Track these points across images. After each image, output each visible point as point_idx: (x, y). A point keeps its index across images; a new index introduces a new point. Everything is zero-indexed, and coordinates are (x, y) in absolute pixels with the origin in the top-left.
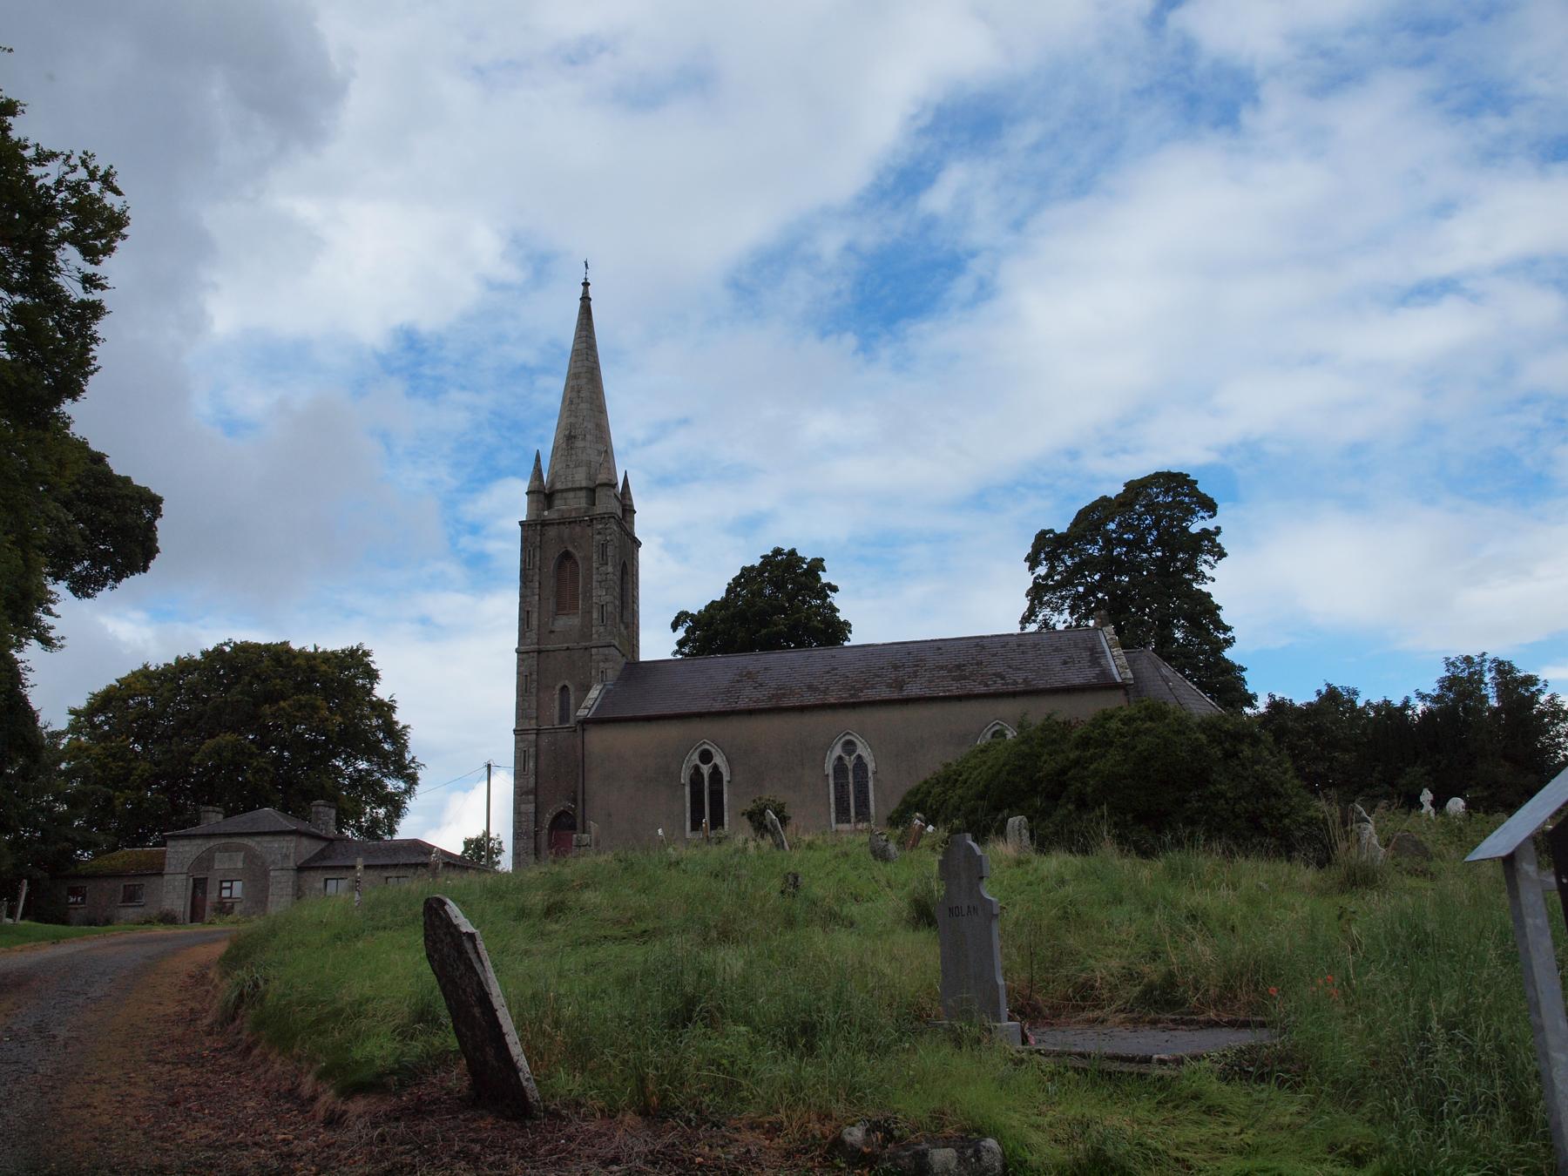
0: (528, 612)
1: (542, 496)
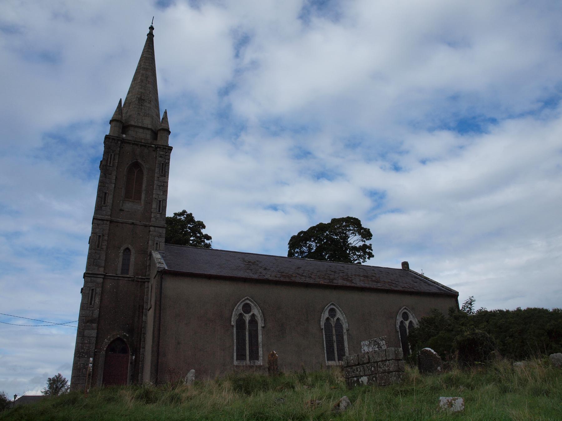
0: (106, 193)
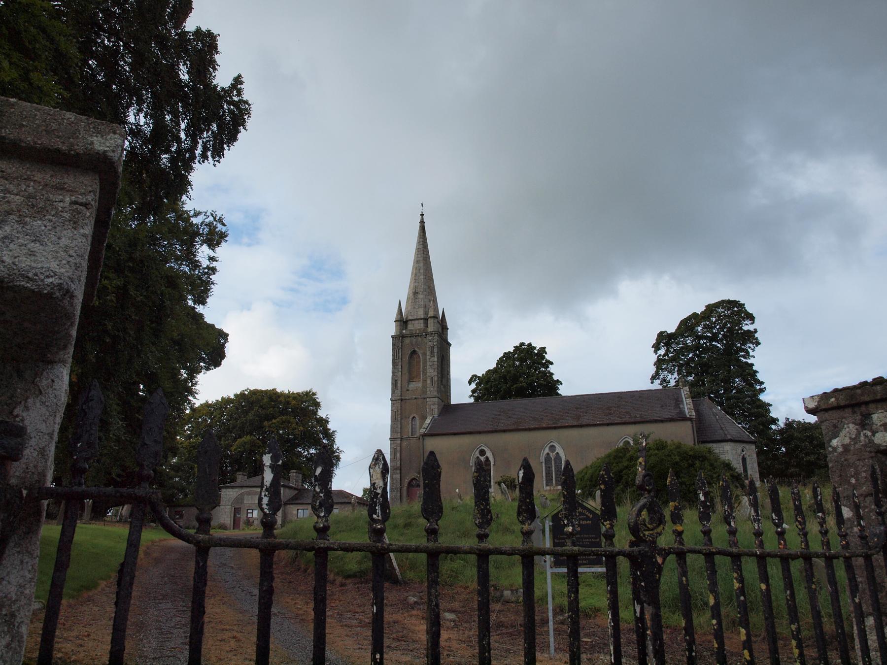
1: (402, 323)
